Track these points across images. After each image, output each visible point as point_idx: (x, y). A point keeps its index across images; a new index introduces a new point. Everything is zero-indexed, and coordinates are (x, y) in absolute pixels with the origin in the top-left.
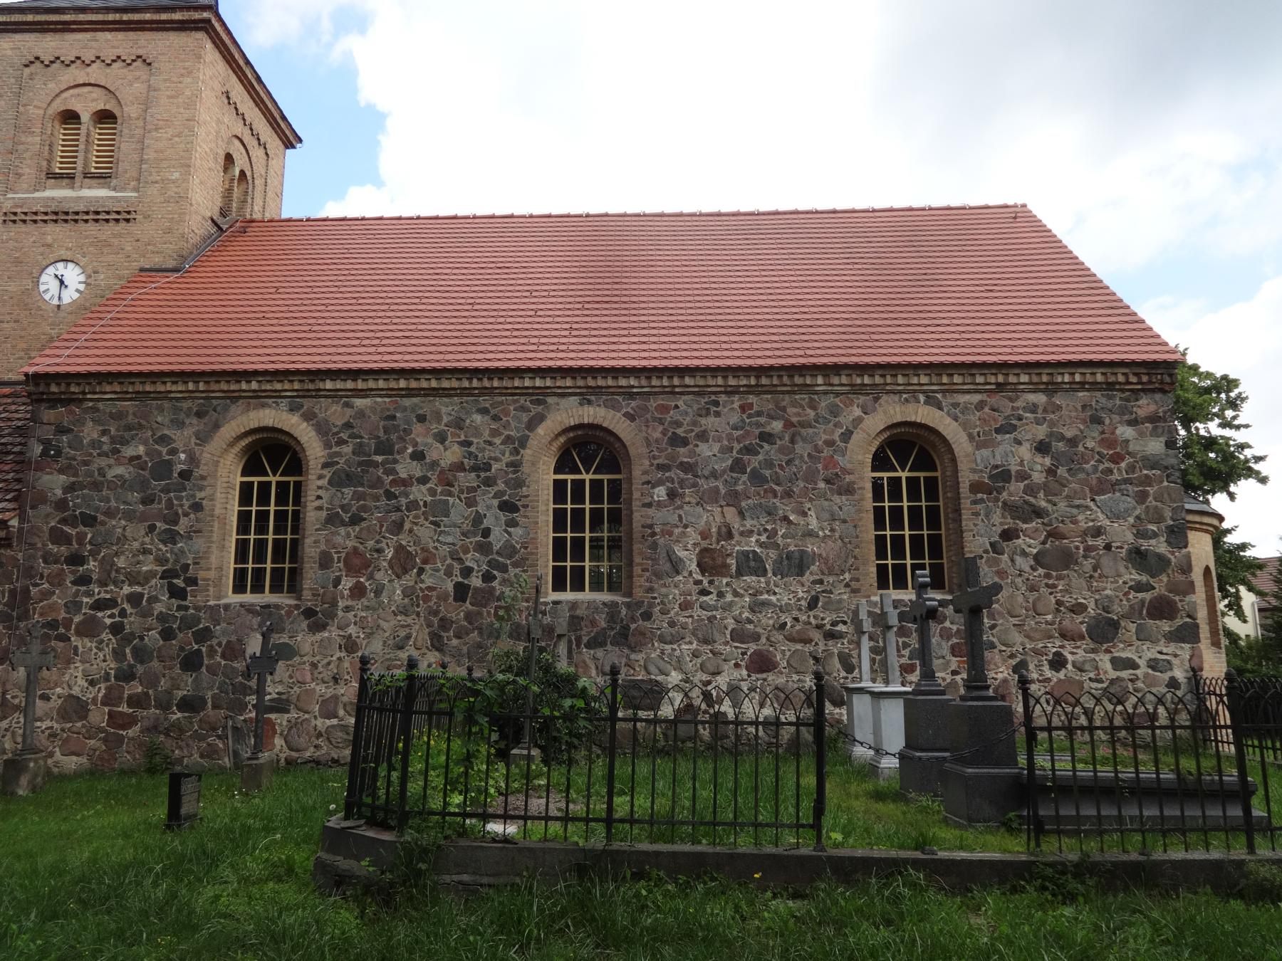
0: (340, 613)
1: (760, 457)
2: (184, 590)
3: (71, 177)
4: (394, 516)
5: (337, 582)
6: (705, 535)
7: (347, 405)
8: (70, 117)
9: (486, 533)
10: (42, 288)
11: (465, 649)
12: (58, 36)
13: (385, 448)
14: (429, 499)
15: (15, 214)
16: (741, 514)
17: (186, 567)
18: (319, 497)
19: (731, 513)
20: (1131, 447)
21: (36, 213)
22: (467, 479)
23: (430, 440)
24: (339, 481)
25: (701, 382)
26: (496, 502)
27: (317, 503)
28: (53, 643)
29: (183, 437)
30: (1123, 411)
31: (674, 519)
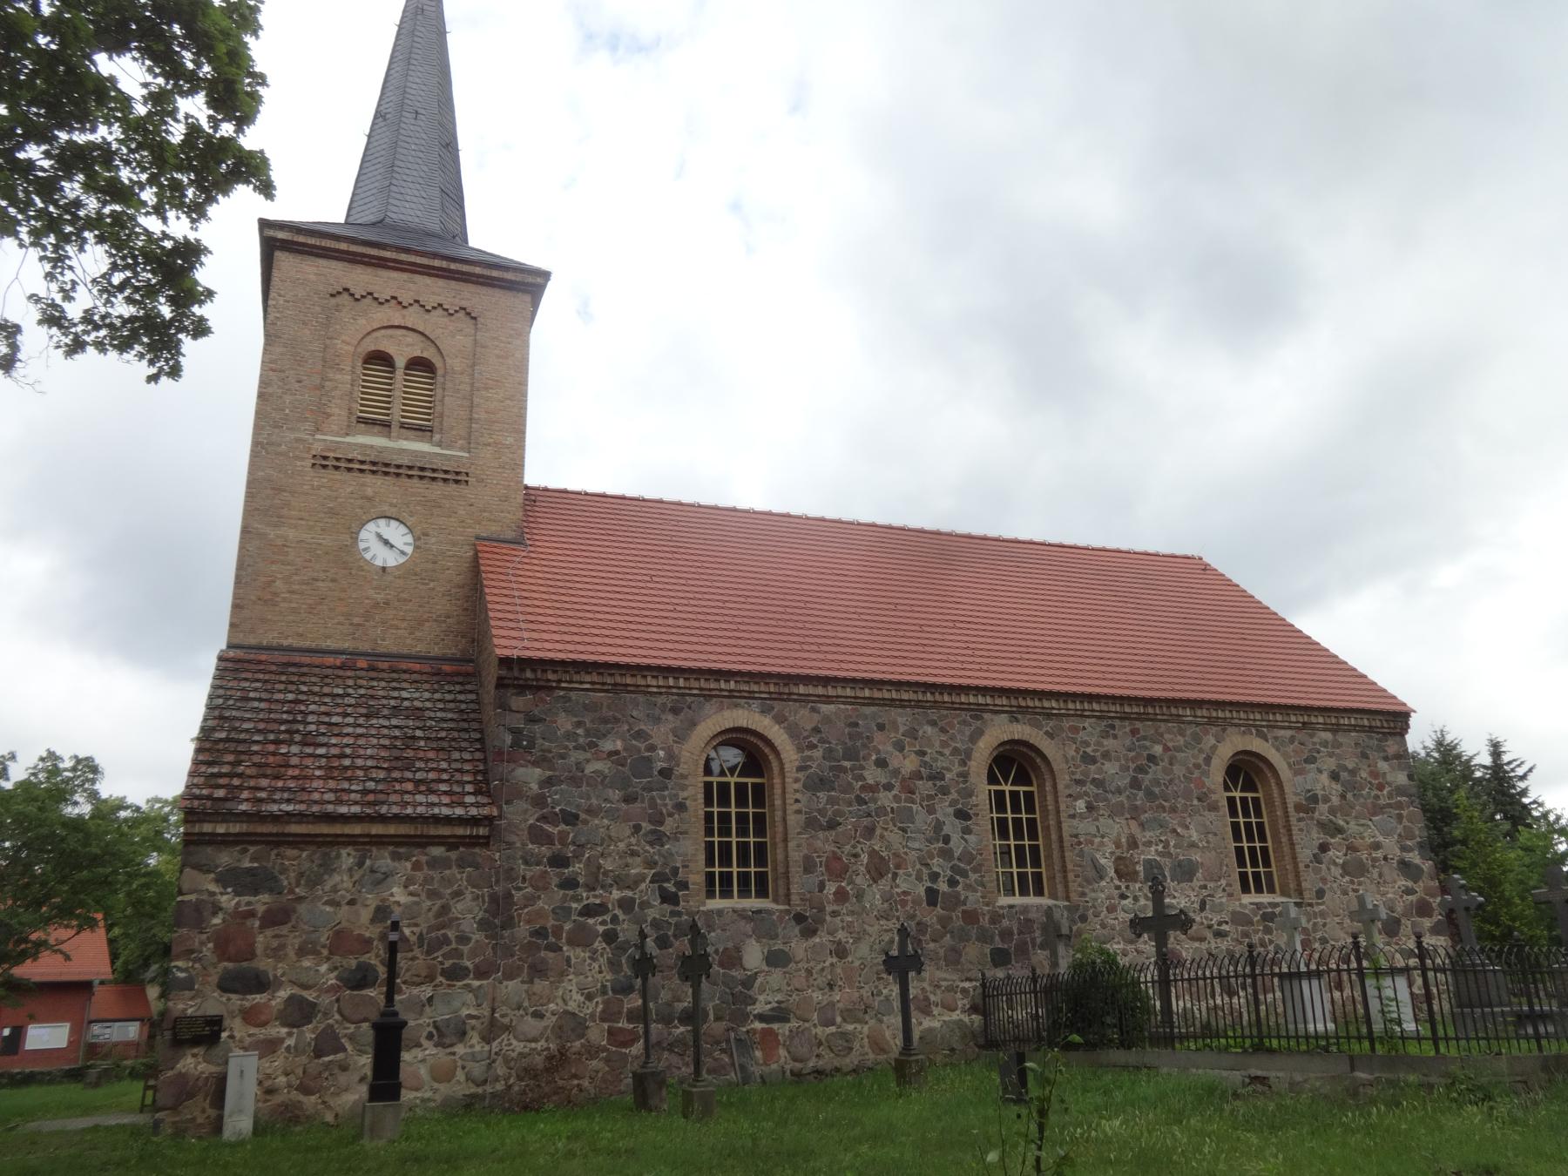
0: (828, 918)
1: (1149, 776)
2: (676, 895)
3: (387, 425)
4: (866, 821)
5: (822, 886)
6: (1118, 845)
7: (813, 710)
8: (380, 359)
9: (947, 840)
10: (362, 545)
11: (942, 952)
12: (369, 270)
13: (851, 754)
14: (895, 805)
15: (325, 458)
16: (1142, 825)
17: (675, 871)
18: (797, 801)
19: (1134, 827)
20: (1389, 778)
21: (350, 461)
22: (925, 787)
23: (890, 749)
24: (816, 784)
25: (1105, 708)
26: (951, 810)
27: (797, 806)
28: (543, 954)
29: (660, 733)
30: (1381, 749)
31: (1093, 830)
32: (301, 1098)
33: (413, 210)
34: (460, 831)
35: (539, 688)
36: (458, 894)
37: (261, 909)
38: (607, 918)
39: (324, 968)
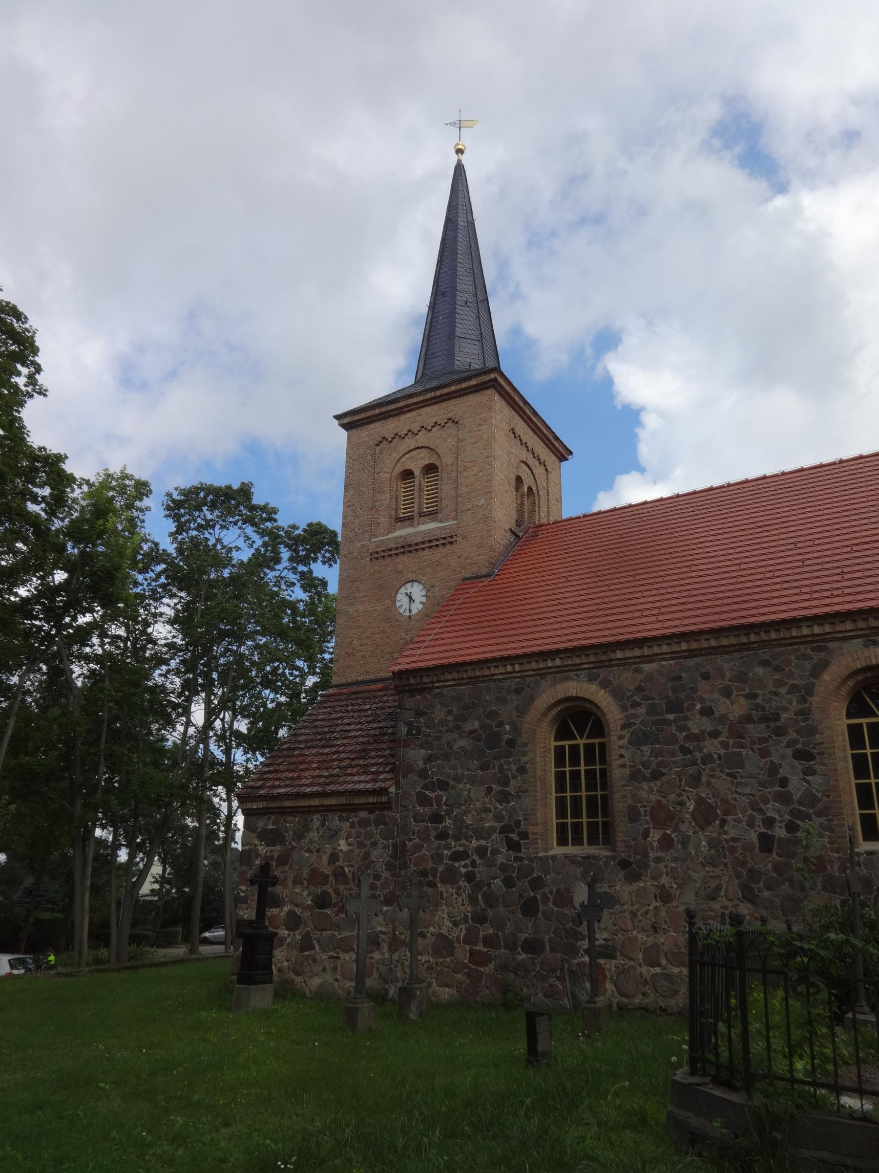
0: (652, 864)
2: (518, 843)
4: (691, 770)
7: (637, 671)
8: (408, 474)
9: (784, 782)
10: (398, 604)
11: (778, 901)
12: (395, 419)
13: (675, 707)
15: (377, 553)
18: (621, 756)
22: (757, 730)
23: (716, 696)
24: (639, 739)
26: (789, 752)
32: (294, 977)
33: (467, 356)
34: (371, 800)
35: (424, 689)
36: (375, 844)
37: (276, 854)
38: (468, 862)
39: (305, 894)
